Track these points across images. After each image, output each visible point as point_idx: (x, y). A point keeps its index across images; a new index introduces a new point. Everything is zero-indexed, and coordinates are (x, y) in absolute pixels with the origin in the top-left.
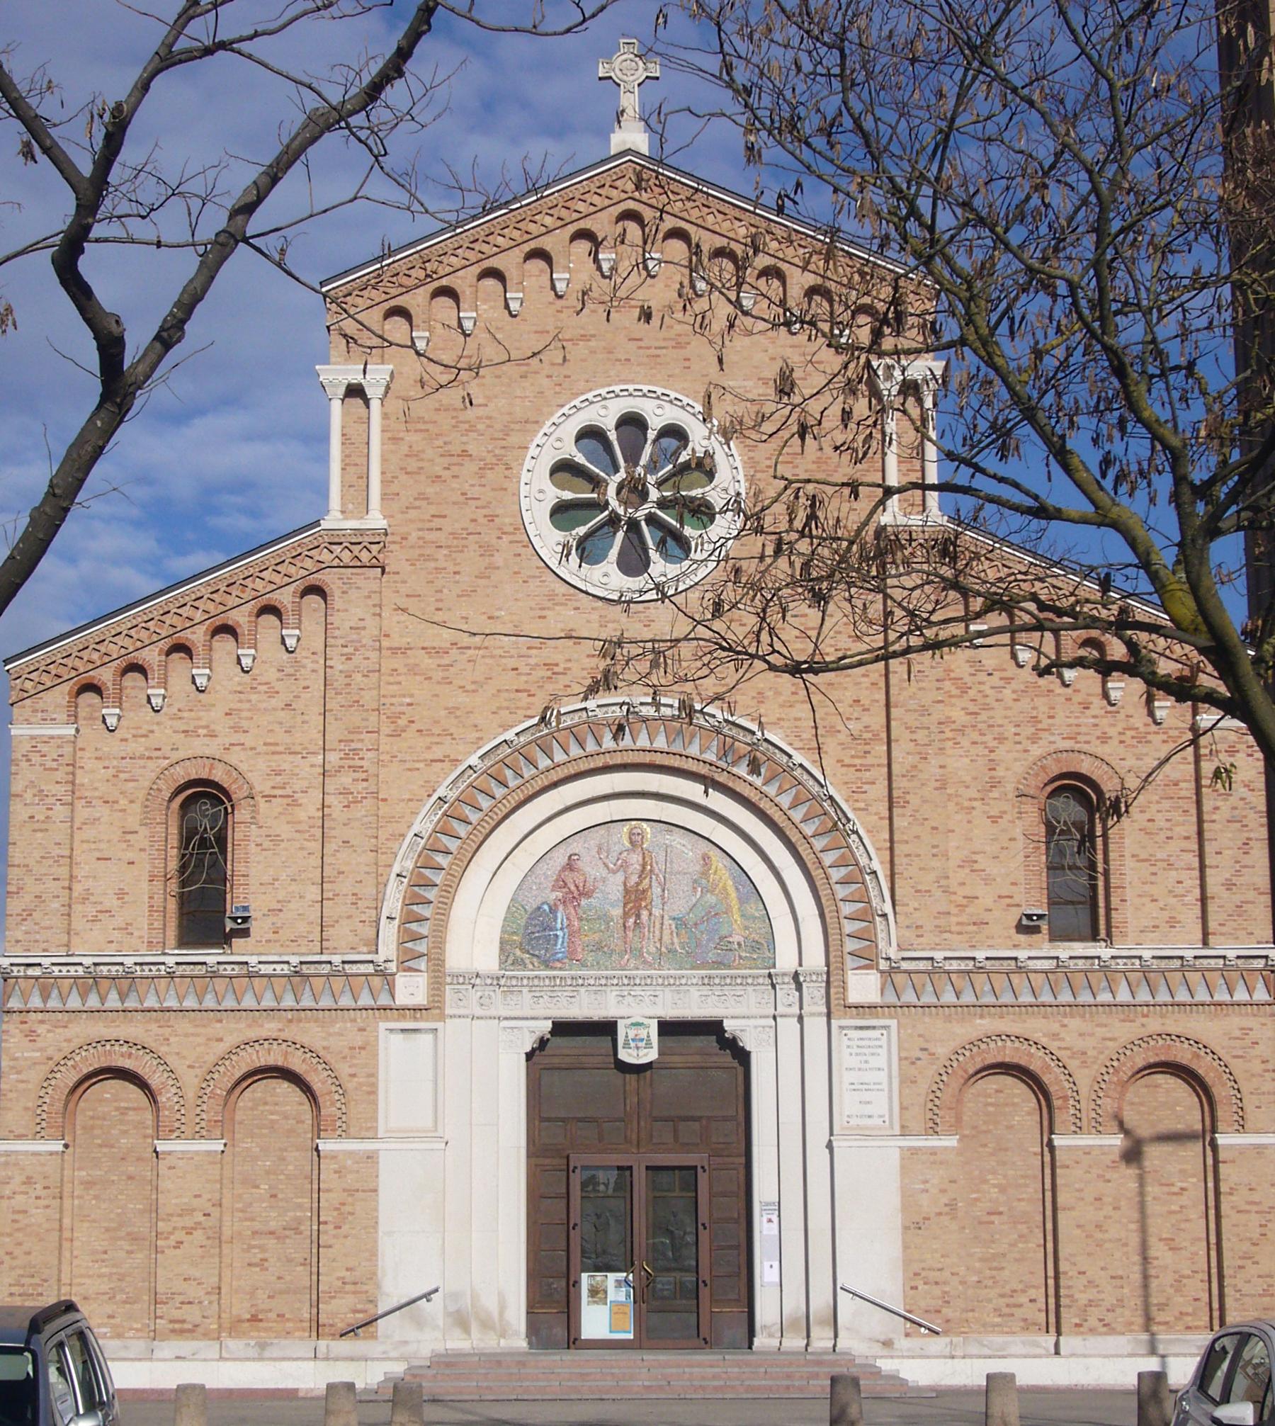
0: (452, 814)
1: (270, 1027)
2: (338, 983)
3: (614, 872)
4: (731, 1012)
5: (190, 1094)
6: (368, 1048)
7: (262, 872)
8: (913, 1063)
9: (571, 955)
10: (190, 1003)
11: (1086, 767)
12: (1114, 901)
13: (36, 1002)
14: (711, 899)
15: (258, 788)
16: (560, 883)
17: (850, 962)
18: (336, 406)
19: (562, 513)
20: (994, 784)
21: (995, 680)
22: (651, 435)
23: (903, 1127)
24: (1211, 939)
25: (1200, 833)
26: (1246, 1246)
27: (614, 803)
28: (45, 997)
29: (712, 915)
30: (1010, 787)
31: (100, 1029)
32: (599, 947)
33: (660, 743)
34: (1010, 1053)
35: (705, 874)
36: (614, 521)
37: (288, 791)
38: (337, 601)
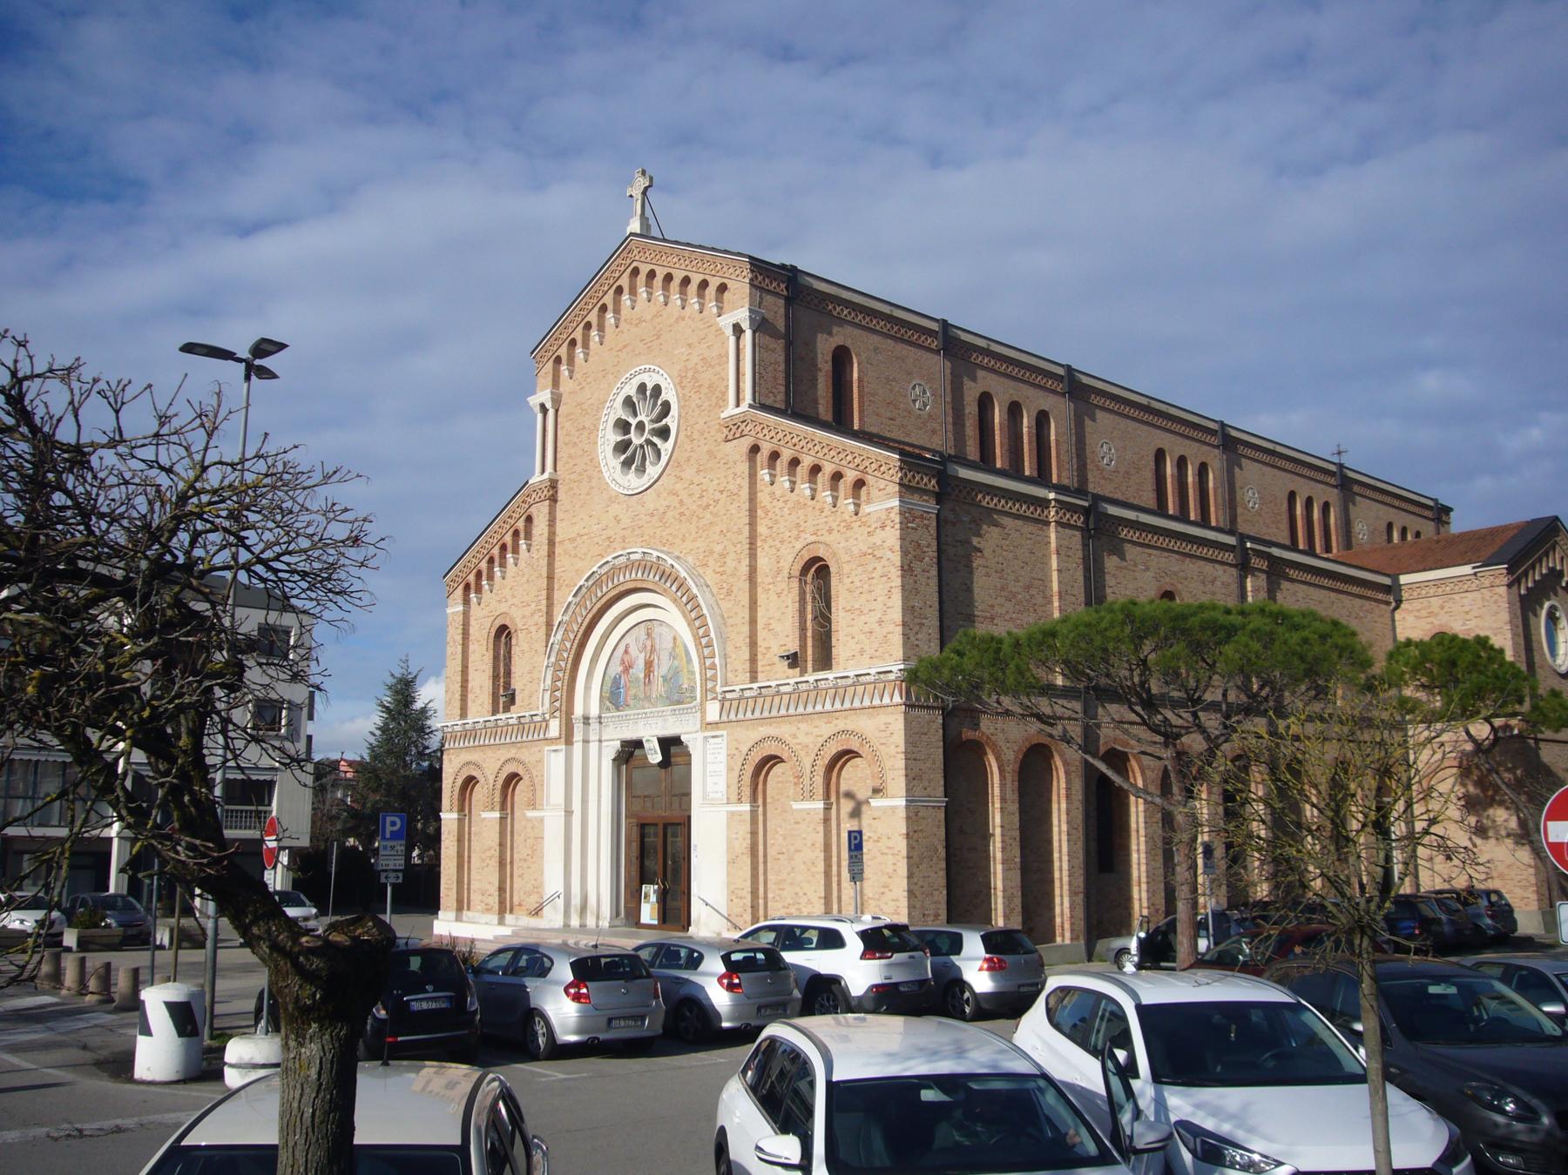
6: (540, 761)
16: (623, 662)
26: (885, 879)
32: (635, 697)
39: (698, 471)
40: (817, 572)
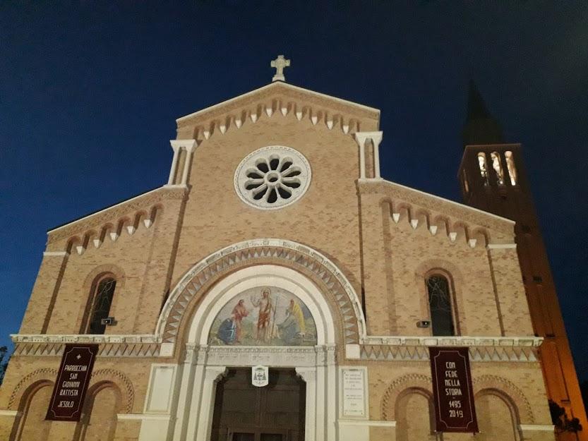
3: (256, 307)
4: (298, 365)
6: (145, 375)
8: (375, 386)
12: (460, 319)
14: (292, 317)
15: (127, 274)
16: (235, 311)
21: (404, 234)
23: (370, 416)
24: (506, 333)
25: (495, 291)
30: (412, 273)
32: (247, 337)
35: (291, 308)
37: (137, 276)
39: (327, 207)
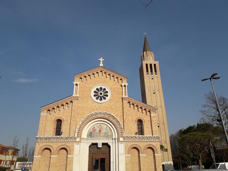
0: (83, 122)
1: (64, 144)
2: (71, 139)
5: (55, 150)
6: (73, 146)
7: (64, 128)
9: (94, 136)
10: (56, 141)
11: (141, 119)
12: (144, 131)
13: (40, 141)
16: (93, 129)
17: (120, 137)
18: (75, 85)
19: (95, 96)
20: (133, 120)
22: (103, 89)
27: (96, 122)
28: (41, 141)
29: (107, 133)
31: (46, 144)
33: (103, 116)
34: (135, 146)
36: (101, 97)
38: (73, 102)
40: (140, 122)
